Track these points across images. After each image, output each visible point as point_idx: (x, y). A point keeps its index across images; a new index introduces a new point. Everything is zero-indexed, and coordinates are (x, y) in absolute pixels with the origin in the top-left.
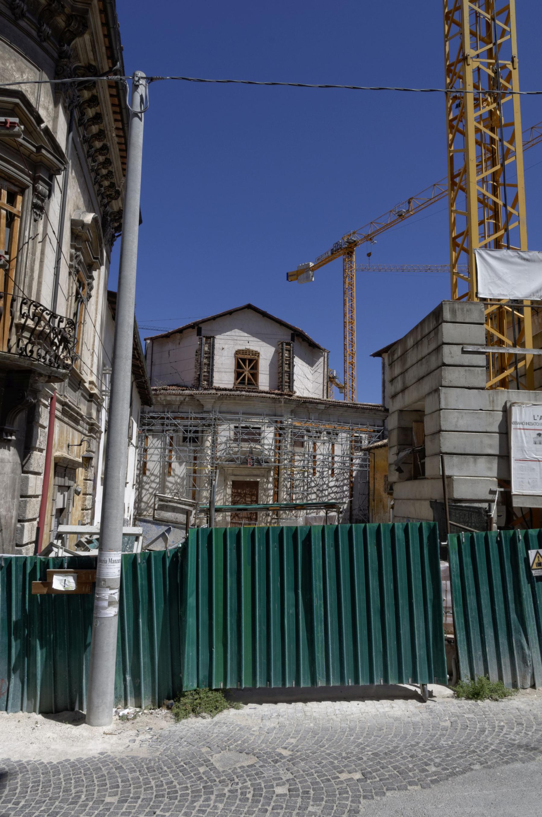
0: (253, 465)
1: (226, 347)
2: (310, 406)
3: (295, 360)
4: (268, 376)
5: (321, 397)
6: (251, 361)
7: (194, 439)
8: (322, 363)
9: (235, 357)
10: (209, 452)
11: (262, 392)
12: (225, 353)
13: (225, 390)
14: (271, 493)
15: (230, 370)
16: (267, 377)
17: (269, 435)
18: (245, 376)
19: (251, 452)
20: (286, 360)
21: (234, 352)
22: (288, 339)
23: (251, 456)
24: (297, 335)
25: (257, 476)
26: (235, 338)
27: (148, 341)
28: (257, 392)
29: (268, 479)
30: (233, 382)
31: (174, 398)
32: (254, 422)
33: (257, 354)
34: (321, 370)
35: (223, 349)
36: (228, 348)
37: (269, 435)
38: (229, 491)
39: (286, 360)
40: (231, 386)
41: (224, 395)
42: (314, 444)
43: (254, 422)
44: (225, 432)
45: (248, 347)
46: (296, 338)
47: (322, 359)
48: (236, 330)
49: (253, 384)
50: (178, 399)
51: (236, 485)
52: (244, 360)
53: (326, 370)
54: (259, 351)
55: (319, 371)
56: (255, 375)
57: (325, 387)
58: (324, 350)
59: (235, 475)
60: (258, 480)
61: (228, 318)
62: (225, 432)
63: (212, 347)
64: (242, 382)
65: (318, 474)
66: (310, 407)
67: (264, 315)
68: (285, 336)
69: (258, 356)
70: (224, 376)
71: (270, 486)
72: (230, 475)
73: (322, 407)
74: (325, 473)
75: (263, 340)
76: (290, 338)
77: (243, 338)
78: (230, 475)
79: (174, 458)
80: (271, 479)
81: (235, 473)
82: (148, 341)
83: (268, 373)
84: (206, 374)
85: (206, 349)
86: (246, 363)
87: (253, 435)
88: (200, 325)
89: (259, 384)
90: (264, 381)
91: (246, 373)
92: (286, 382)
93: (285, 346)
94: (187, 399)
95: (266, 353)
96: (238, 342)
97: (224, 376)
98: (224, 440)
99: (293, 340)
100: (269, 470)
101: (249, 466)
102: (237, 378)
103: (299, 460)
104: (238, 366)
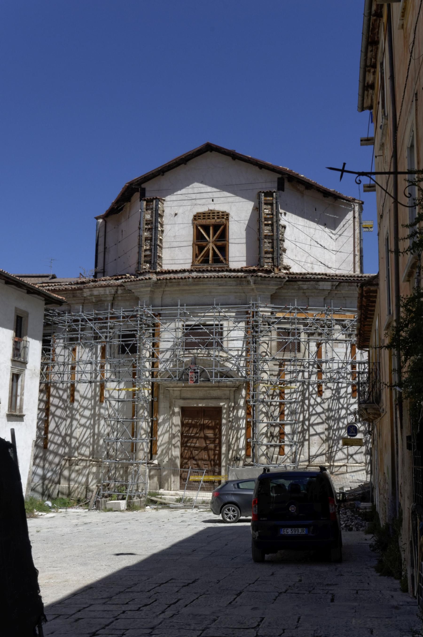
0: (196, 381)
1: (180, 211)
2: (305, 286)
3: (136, 193)
4: (244, 246)
5: (352, 273)
6: (216, 227)
7: (128, 347)
8: (351, 222)
9: (193, 224)
10: (148, 365)
11: (234, 271)
12: (179, 219)
13: (184, 271)
14: (243, 423)
15: (185, 244)
16: (243, 248)
17: (235, 337)
18: (208, 250)
19: (194, 362)
20: (266, 219)
21: (191, 217)
22: (273, 186)
23: (193, 367)
24: (287, 181)
25: (219, 399)
26: (194, 196)
27: (101, 221)
28: (227, 271)
29: (236, 403)
30: (191, 261)
31: (101, 291)
32: (209, 317)
33: (225, 216)
34: (349, 233)
35: (176, 214)
36: (184, 213)
37: (235, 337)
38: (177, 420)
39: (266, 219)
40: (188, 267)
41: (173, 280)
42: (319, 345)
43: (209, 317)
44: (170, 335)
45: (212, 207)
46: (287, 185)
47: (350, 215)
48: (196, 185)
49: (221, 262)
50: (108, 292)
51: (185, 412)
52: (206, 228)
53: (357, 231)
54: (228, 211)
55: (345, 234)
56: (223, 249)
57: (357, 258)
58: (350, 201)
59: (184, 399)
60: (222, 404)
61: (181, 171)
62: (170, 335)
63: (158, 215)
64: (206, 261)
65: (327, 394)
66: (305, 287)
67: (234, 156)
68: (269, 182)
69: (227, 219)
70: (177, 252)
71: (242, 413)
72: (176, 398)
73: (327, 286)
74: (343, 391)
75: (236, 193)
76: (276, 185)
77: (205, 195)
78: (176, 398)
79: (107, 375)
80: (242, 402)
81: (184, 395)
82: (101, 221)
83: (244, 241)
84: (148, 253)
85: (148, 217)
86: (211, 230)
87: (202, 336)
88: (143, 186)
89: (230, 259)
90: (238, 256)
91: (211, 246)
92: (266, 253)
93: (263, 198)
94: (120, 292)
95: (239, 212)
96: (198, 202)
97: (177, 252)
98: (169, 345)
99: (281, 187)
100: (238, 389)
101: (190, 383)
102: (196, 256)
103: (290, 372)
104: (199, 237)
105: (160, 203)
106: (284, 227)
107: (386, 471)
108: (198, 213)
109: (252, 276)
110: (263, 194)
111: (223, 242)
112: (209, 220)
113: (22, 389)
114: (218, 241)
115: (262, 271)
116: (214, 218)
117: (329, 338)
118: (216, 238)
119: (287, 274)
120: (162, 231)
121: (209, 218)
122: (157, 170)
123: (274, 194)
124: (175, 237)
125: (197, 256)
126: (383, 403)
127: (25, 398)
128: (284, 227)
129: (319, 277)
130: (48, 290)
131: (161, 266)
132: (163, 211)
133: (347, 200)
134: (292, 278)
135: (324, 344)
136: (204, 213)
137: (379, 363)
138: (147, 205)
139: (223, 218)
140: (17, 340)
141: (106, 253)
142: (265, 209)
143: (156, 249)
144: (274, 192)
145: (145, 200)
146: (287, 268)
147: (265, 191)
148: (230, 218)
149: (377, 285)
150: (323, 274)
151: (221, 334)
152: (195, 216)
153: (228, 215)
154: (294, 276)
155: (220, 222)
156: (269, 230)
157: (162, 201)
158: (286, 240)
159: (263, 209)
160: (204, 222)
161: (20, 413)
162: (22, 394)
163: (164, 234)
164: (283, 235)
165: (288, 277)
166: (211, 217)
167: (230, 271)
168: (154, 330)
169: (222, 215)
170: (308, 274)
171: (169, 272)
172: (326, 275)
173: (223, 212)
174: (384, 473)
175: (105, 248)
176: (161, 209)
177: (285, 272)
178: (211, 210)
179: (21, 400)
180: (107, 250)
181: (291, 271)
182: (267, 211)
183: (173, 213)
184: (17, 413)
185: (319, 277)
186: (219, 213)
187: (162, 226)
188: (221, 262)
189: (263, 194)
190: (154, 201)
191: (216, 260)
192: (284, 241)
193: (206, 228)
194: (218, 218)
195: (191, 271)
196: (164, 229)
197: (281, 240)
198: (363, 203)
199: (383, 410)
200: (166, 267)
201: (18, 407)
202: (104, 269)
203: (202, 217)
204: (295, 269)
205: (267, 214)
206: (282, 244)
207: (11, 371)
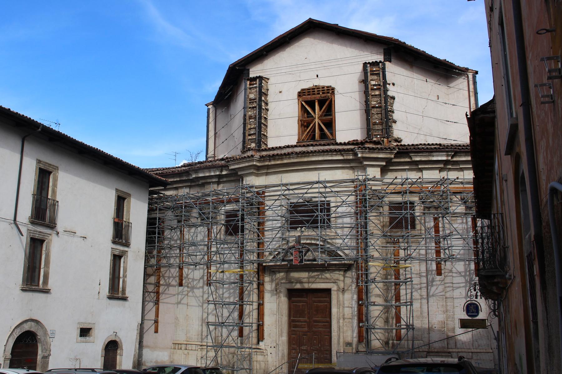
11: (341, 144)
12: (283, 97)
21: (296, 96)
28: (333, 144)
33: (331, 90)
40: (294, 143)
45: (316, 84)
69: (333, 93)
91: (317, 120)
105: (263, 81)
106: (393, 98)
107: (517, 362)
108: (303, 90)
109: (360, 147)
110: (369, 65)
111: (329, 117)
112: (314, 96)
113: (125, 271)
114: (325, 116)
115: (371, 142)
116: (319, 94)
117: (446, 212)
118: (323, 112)
119: (397, 145)
120: (267, 110)
121: (314, 94)
122: (300, 110)
123: (380, 64)
124: (280, 114)
125: (303, 133)
126: (509, 267)
127: (128, 280)
128: (393, 98)
129: (433, 147)
130: (157, 174)
131: (266, 145)
132: (268, 90)
133: (459, 70)
134: (403, 149)
135: (441, 219)
136: (309, 89)
137: (502, 214)
138: (250, 85)
139: (328, 93)
140: (116, 220)
141: (217, 138)
142: (371, 80)
143: (260, 127)
144: (380, 62)
145: (248, 80)
146: (398, 140)
147: (371, 61)
148: (336, 92)
149: (494, 112)
150: (436, 144)
151: (329, 210)
152: (299, 93)
153: (333, 89)
154: (405, 148)
155: (325, 97)
156: (377, 101)
157: (266, 80)
158: (395, 111)
159: (369, 80)
160: (309, 98)
161: (122, 295)
162: (125, 276)
163: (269, 113)
164: (392, 106)
165: (399, 148)
166: (316, 92)
167: (337, 144)
168: (258, 208)
169: (327, 90)
170: (421, 144)
171: (273, 149)
172: (440, 145)
173: (327, 87)
174: (516, 364)
175: (215, 134)
176: (265, 87)
177: (395, 144)
178: (316, 86)
179: (124, 281)
180: (217, 135)
181: (403, 143)
182: (373, 83)
183: (278, 91)
184: (120, 295)
185: (433, 147)
186: (323, 88)
187: (267, 104)
188: (306, 102)
189: (369, 65)
190: (258, 80)
191: (323, 136)
192: (393, 112)
193: (311, 104)
194: (323, 93)
195: (296, 146)
196: (268, 107)
197: (390, 111)
198: (477, 73)
199: (511, 276)
200: (270, 145)
201: (121, 289)
202: (214, 154)
203: (306, 94)
204: (407, 141)
205: (374, 85)
206: (392, 116)
207: (112, 252)
